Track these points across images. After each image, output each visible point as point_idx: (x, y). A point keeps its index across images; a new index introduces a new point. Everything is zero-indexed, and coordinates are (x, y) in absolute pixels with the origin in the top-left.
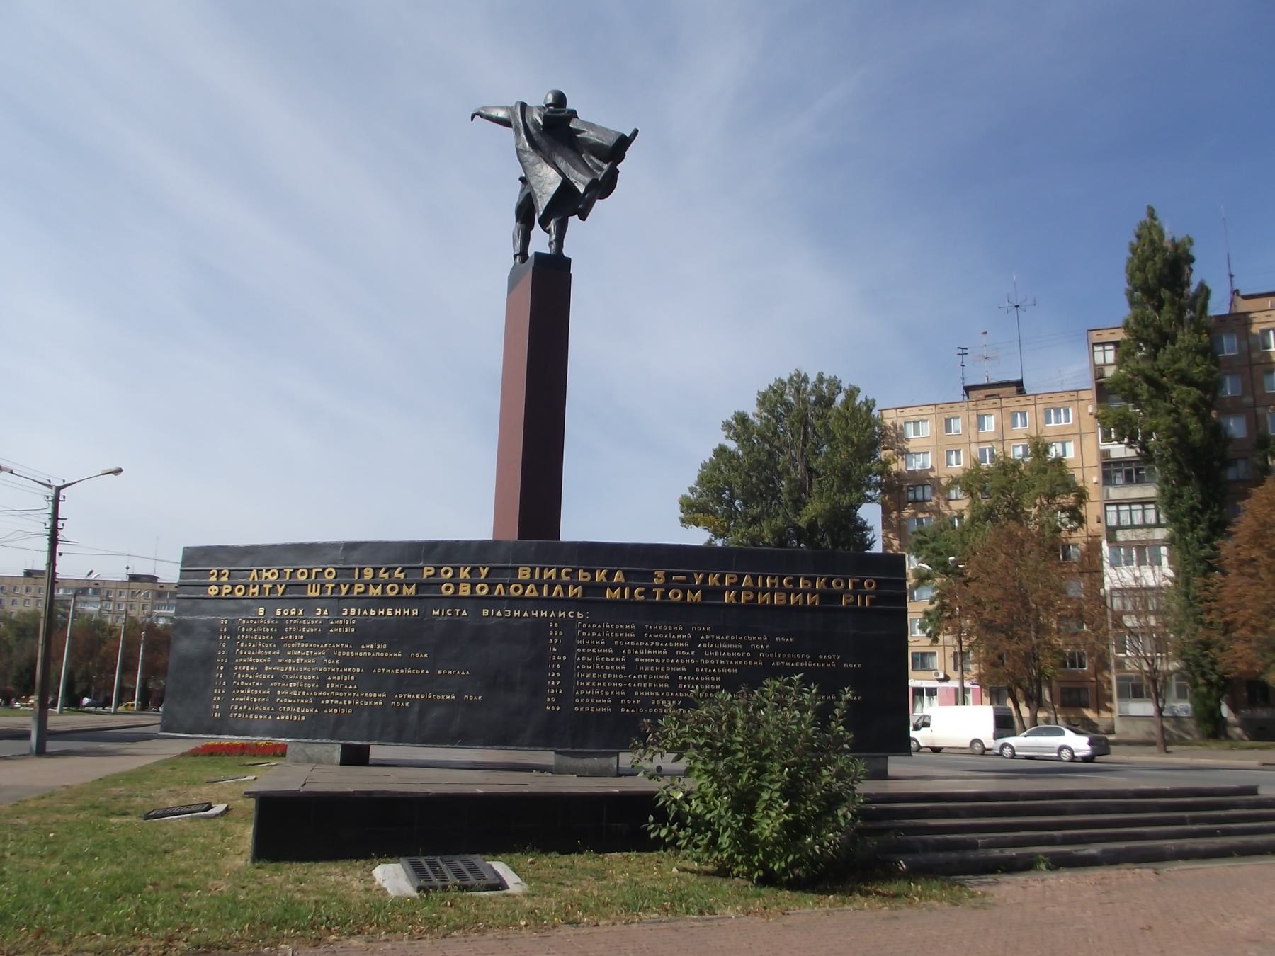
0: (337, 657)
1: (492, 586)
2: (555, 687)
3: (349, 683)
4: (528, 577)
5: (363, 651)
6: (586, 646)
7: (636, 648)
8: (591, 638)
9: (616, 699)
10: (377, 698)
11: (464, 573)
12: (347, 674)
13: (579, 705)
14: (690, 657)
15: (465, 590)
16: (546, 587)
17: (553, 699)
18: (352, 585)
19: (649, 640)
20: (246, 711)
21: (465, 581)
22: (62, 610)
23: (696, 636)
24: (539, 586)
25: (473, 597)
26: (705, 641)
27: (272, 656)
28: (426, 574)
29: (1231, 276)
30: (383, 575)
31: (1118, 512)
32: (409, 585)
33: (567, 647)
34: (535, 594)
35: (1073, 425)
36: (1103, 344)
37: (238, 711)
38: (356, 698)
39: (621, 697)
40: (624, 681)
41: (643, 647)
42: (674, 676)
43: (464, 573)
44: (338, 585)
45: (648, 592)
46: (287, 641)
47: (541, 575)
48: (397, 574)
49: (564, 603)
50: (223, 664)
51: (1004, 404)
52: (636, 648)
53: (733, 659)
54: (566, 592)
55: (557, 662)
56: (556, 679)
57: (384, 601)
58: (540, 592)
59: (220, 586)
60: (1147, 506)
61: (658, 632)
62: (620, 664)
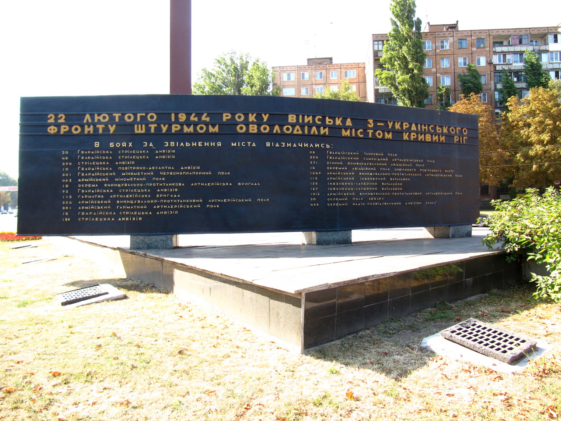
0: (163, 176)
1: (272, 126)
2: (315, 191)
3: (174, 193)
4: (295, 121)
5: (182, 171)
6: (332, 166)
7: (359, 166)
8: (334, 161)
9: (350, 197)
10: (196, 202)
11: (252, 118)
13: (330, 202)
14: (387, 172)
15: (253, 129)
16: (306, 127)
17: (315, 199)
18: (170, 126)
19: (366, 162)
20: (92, 216)
21: (253, 123)
22: (402, 65)
23: (390, 158)
24: (302, 127)
25: (259, 133)
26: (395, 162)
27: (109, 177)
28: (225, 119)
30: (193, 118)
32: (214, 126)
33: (322, 165)
34: (300, 132)
36: (378, 41)
37: (85, 216)
38: (180, 203)
39: (353, 196)
40: (354, 186)
41: (363, 166)
42: (379, 182)
43: (252, 118)
44: (159, 125)
45: (365, 132)
46: (122, 166)
48: (204, 118)
49: (320, 138)
50: (68, 183)
51: (327, 67)
52: (359, 166)
53: (408, 172)
54: (319, 131)
55: (315, 175)
56: (315, 186)
57: (195, 136)
58: (303, 130)
59: (58, 126)
61: (370, 157)
62: (351, 176)
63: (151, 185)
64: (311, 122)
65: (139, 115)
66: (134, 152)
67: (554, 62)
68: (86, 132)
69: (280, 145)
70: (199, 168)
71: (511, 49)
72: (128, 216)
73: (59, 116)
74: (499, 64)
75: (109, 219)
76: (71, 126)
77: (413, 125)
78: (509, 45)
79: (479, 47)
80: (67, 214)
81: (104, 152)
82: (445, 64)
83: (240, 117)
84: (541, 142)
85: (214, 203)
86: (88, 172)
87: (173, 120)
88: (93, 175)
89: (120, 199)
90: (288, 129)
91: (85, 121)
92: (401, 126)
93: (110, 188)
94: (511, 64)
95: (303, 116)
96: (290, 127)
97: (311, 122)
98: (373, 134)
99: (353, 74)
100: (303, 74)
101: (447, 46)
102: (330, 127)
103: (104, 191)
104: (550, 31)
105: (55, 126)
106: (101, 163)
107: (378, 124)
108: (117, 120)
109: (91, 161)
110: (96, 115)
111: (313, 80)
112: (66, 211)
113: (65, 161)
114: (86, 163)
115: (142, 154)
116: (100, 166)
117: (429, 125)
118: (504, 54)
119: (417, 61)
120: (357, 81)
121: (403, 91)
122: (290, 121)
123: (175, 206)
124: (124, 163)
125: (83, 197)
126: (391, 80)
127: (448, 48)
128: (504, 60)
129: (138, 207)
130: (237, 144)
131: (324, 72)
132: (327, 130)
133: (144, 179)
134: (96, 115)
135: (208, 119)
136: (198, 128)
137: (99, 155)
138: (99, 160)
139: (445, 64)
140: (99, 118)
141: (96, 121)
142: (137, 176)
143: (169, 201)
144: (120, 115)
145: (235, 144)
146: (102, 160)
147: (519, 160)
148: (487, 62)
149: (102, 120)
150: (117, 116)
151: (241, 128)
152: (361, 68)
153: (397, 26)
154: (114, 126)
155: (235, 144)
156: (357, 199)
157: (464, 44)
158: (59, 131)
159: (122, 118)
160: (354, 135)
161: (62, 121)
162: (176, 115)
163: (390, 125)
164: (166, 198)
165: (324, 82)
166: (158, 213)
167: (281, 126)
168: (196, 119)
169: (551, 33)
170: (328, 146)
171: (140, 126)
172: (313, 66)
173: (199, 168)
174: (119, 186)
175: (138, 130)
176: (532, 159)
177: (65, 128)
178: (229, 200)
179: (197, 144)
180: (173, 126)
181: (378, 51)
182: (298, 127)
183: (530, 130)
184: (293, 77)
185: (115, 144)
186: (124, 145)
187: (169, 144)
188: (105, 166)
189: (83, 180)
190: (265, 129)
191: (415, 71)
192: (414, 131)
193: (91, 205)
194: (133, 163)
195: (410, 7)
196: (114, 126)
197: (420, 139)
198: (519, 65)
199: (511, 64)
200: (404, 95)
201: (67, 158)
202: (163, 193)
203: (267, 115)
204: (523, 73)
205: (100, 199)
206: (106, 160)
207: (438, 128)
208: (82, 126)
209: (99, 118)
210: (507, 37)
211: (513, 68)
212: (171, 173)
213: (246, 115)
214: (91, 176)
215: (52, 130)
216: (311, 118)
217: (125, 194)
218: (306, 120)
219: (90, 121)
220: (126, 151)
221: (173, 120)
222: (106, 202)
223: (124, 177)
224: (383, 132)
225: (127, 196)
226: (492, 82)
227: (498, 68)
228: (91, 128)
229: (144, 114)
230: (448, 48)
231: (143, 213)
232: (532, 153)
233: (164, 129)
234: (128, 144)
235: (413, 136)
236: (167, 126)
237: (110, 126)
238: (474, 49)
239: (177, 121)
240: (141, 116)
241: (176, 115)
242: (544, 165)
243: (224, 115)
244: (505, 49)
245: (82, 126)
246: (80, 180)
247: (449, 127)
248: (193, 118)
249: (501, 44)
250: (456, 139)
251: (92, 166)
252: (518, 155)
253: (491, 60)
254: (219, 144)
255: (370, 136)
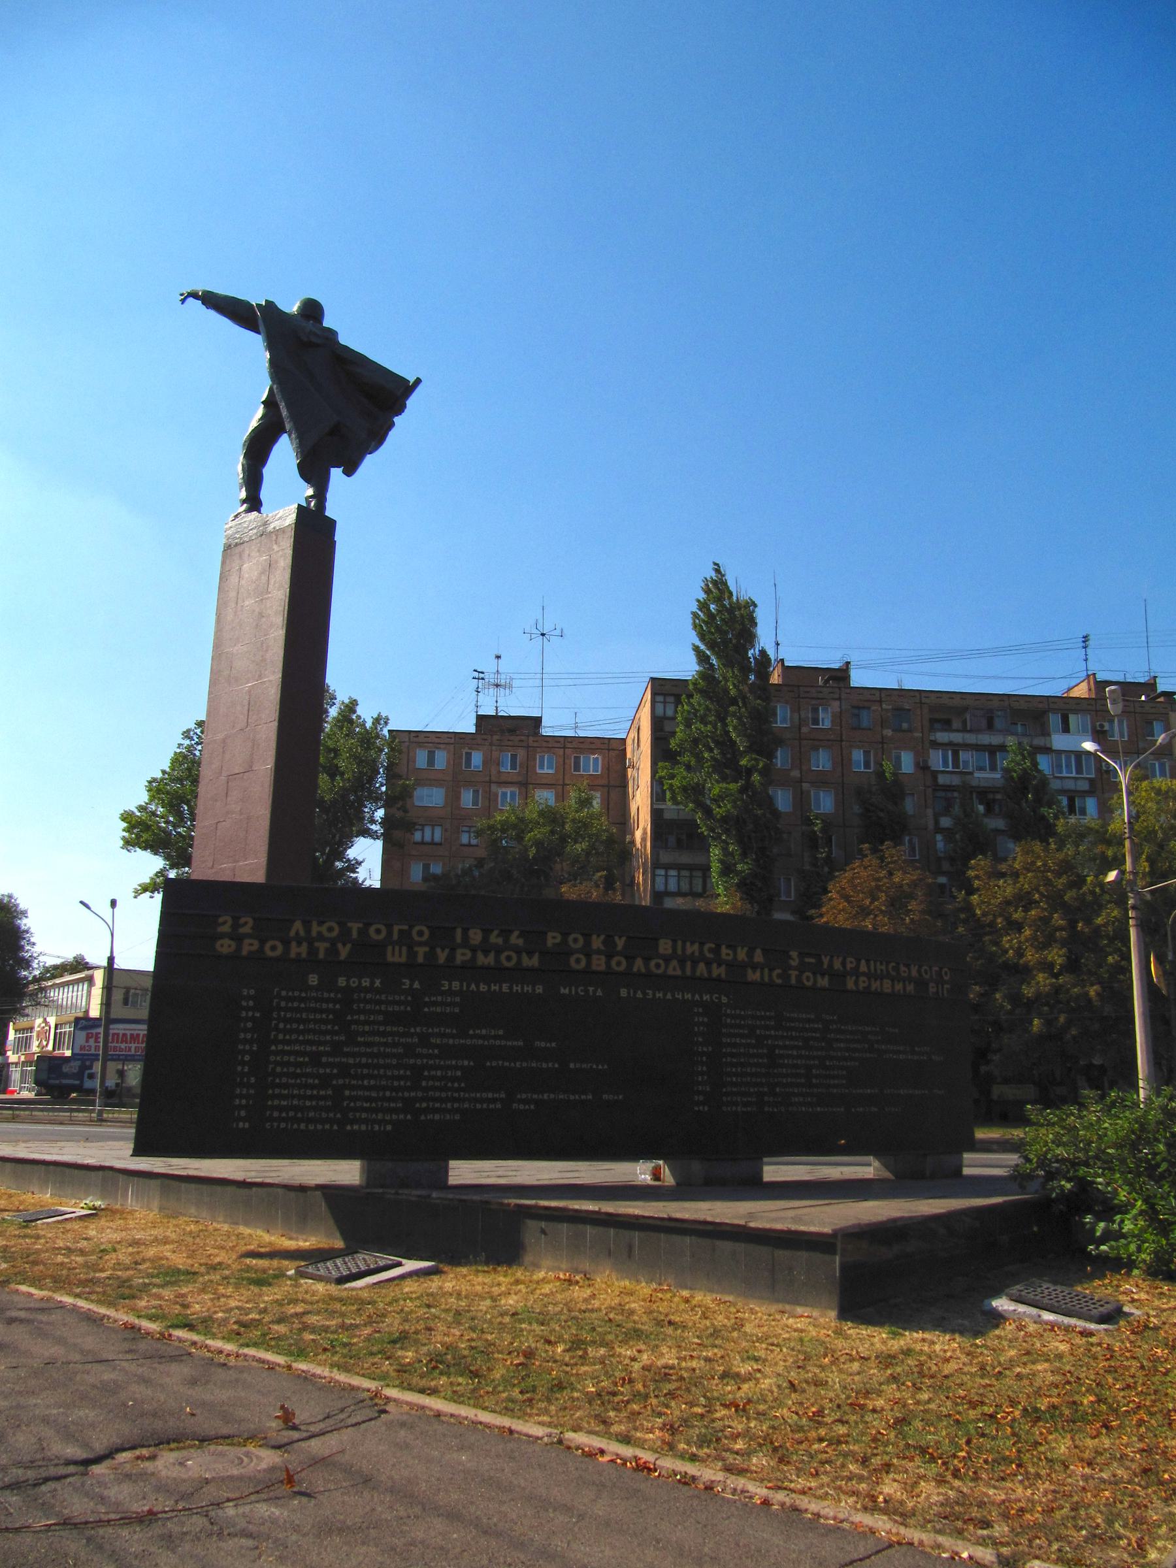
1: (630, 959)
4: (670, 951)
5: (472, 1037)
12: (449, 1067)
15: (599, 963)
16: (689, 964)
18: (453, 950)
21: (599, 952)
24: (682, 962)
28: (550, 942)
29: (778, 644)
30: (495, 939)
31: (666, 876)
34: (679, 972)
35: (601, 776)
43: (597, 942)
44: (433, 949)
46: (357, 1022)
47: (684, 949)
57: (497, 973)
58: (683, 968)
59: (239, 939)
60: (694, 873)
63: (412, 1061)
64: (697, 954)
65: (396, 928)
66: (383, 997)
67: (1065, 774)
68: (293, 955)
69: (645, 994)
70: (501, 1032)
71: (971, 738)
72: (366, 1121)
73: (242, 921)
74: (943, 772)
75: (327, 1127)
76: (263, 942)
77: (863, 962)
78: (964, 730)
79: (899, 730)
80: (243, 1113)
81: (326, 995)
82: (822, 761)
83: (576, 941)
84: (1048, 967)
85: (525, 1102)
86: (291, 1032)
87: (459, 940)
88: (301, 1038)
89: (352, 1088)
90: (658, 966)
91: (292, 933)
92: (844, 964)
93: (331, 1065)
94: (971, 773)
95: (684, 943)
96: (661, 962)
97: (697, 954)
98: (799, 978)
99: (593, 765)
100: (469, 755)
101: (826, 720)
102: (729, 965)
103: (321, 1071)
104: (1052, 706)
105: (232, 939)
106: (318, 1016)
107: (807, 960)
108: (355, 934)
109: (298, 1010)
110: (315, 924)
111: (494, 772)
112: (240, 1107)
113: (248, 1009)
114: (289, 1015)
115: (399, 1003)
116: (316, 1021)
117: (888, 963)
118: (956, 748)
119: (759, 753)
120: (604, 782)
121: (725, 820)
122: (661, 951)
123: (456, 1105)
124: (362, 1017)
125: (277, 1081)
126: (695, 792)
127: (827, 724)
128: (956, 763)
129: (386, 1104)
130: (570, 990)
131: (521, 754)
132: (723, 968)
133: (401, 1050)
134: (315, 924)
135: (520, 942)
136: (503, 957)
137: (317, 1000)
138: (315, 1011)
139: (822, 761)
140: (319, 929)
141: (314, 934)
142: (386, 1044)
143: (444, 1095)
144: (361, 925)
145: (567, 991)
146: (322, 1011)
147: (1002, 1007)
148: (917, 765)
149: (326, 934)
150: (355, 927)
151: (578, 961)
152: (613, 751)
153: (712, 665)
154: (349, 946)
155: (567, 991)
156: (771, 1099)
157: (866, 720)
158: (239, 948)
159: (363, 932)
160: (766, 979)
161: (247, 929)
162: (465, 931)
163: (826, 961)
164: (441, 1089)
165: (520, 779)
166: (423, 1117)
167: (647, 960)
168: (500, 941)
169: (1055, 711)
170: (724, 1000)
171: (397, 948)
172: (496, 737)
173: (501, 1032)
174: (351, 1061)
175: (393, 954)
176: (1030, 1006)
177: (251, 945)
178: (552, 1096)
179: (501, 987)
180: (459, 951)
181: (665, 718)
182: (674, 963)
183: (1022, 939)
184: (442, 759)
185: (348, 981)
186: (366, 982)
187: (450, 985)
188: (326, 1022)
189: (280, 1047)
190: (619, 964)
191: (756, 777)
192: (864, 974)
193: (293, 1097)
194: (381, 1018)
195: (743, 623)
196: (349, 946)
197: (873, 989)
198: (987, 777)
199: (971, 773)
200: (727, 831)
201: (251, 1003)
202: (433, 1078)
203: (624, 939)
204: (999, 796)
205: (313, 1087)
206: (327, 1011)
207: (903, 968)
208: (286, 943)
209: (319, 929)
210: (961, 711)
211: (974, 783)
212: (451, 1042)
213: (587, 936)
214: (297, 1041)
215: (225, 946)
216: (696, 947)
217: (363, 1077)
218: (689, 951)
219: (302, 933)
220: (369, 996)
221: (459, 940)
222: (322, 1093)
223: (359, 1044)
224: (814, 974)
225: (366, 1082)
226: (930, 812)
227: (942, 780)
228: (304, 950)
229: (406, 927)
230: (827, 724)
231: (394, 1117)
232: (1028, 991)
233: (442, 956)
234: (372, 983)
235: (863, 983)
236: (447, 951)
237: (340, 946)
238: (888, 733)
239: (466, 943)
240: (401, 931)
241: (465, 931)
242: (1057, 1018)
243: (550, 934)
244: (957, 737)
245: (286, 943)
246: (273, 1048)
247: (920, 967)
248: (495, 939)
249: (947, 725)
250: (932, 989)
251: (299, 1021)
252: (998, 996)
253: (925, 761)
254: (539, 989)
255: (793, 981)
